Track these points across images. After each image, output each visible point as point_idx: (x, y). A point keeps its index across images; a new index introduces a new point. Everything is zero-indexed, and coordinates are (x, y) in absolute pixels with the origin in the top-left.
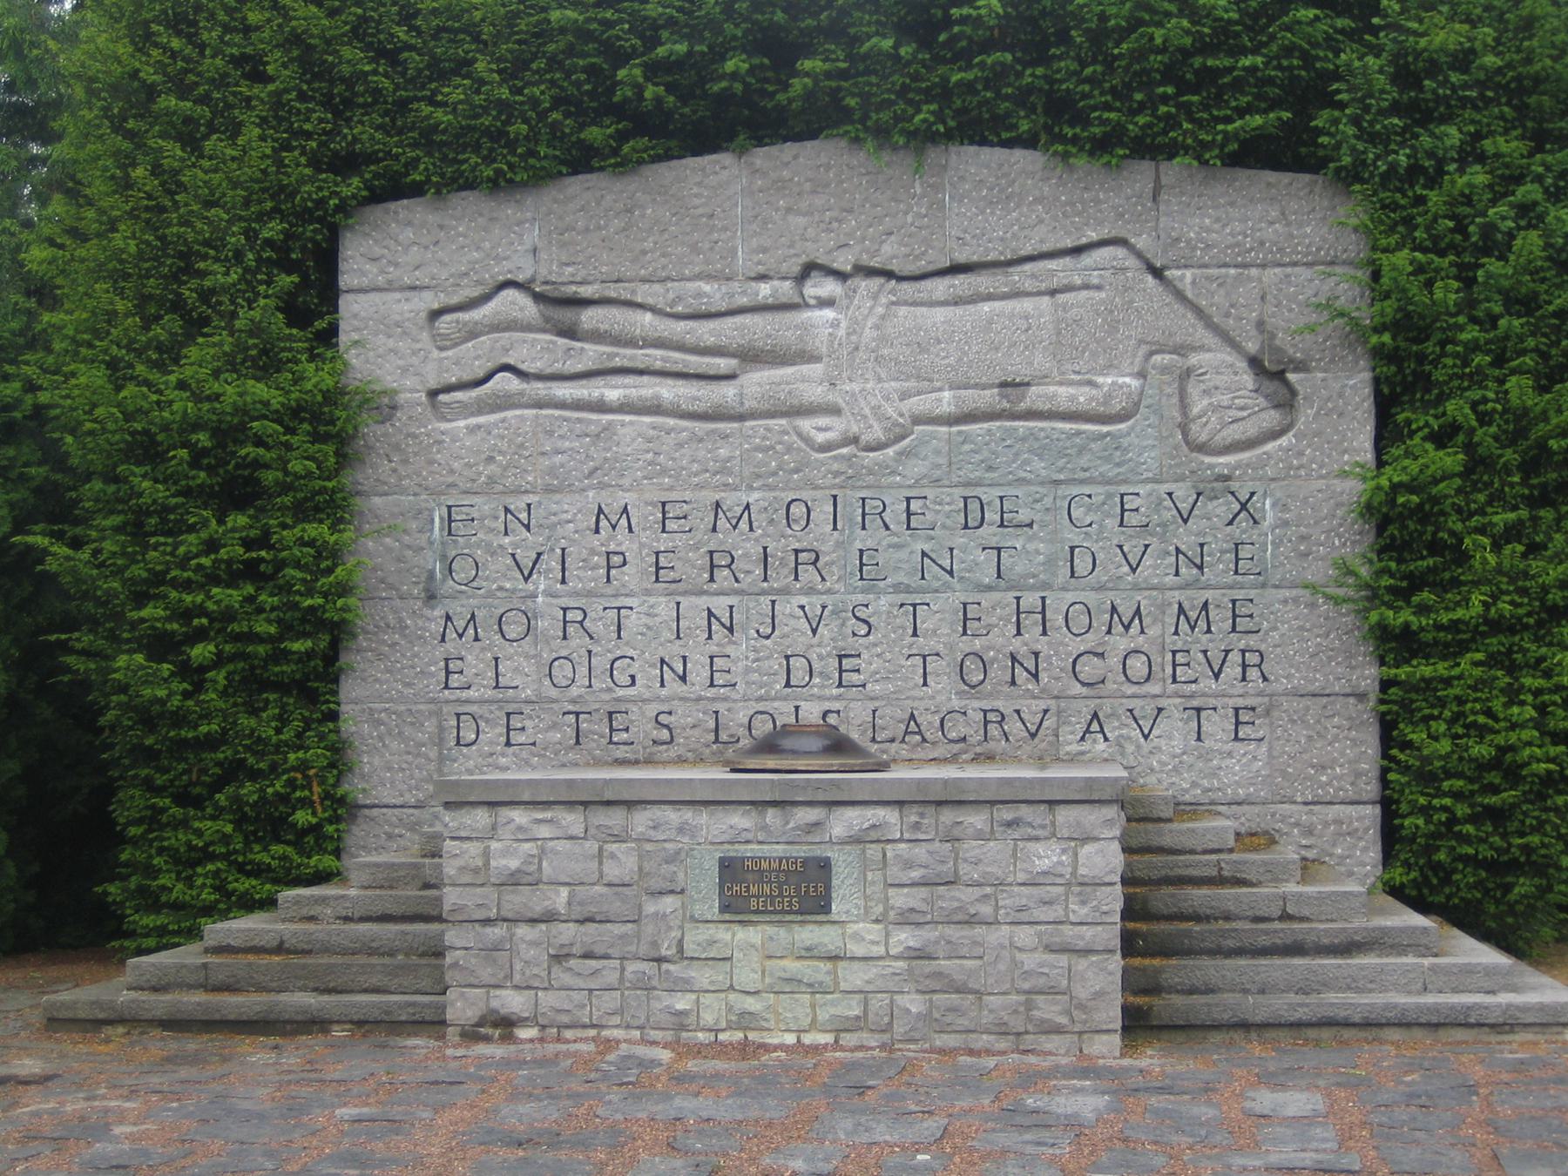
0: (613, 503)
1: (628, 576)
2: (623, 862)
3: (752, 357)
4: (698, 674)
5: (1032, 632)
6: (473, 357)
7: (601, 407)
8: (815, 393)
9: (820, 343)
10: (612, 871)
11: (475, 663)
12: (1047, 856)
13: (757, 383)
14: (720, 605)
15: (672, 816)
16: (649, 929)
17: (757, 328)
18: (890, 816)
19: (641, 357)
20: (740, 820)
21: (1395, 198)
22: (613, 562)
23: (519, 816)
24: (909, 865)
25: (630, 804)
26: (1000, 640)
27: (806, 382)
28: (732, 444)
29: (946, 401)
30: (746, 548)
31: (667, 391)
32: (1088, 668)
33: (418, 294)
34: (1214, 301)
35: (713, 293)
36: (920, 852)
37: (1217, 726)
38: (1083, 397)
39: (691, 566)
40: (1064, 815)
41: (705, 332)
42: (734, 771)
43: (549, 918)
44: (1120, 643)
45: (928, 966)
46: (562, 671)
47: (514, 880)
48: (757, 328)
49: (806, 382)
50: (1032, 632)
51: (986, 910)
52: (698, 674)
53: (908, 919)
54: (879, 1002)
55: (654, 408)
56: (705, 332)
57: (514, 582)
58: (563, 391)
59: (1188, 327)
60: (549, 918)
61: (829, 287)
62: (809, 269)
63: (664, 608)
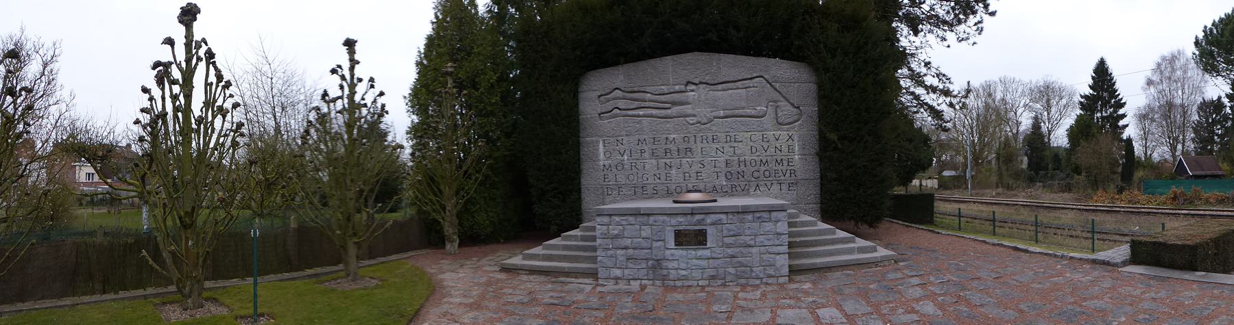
0: (642, 137)
1: (646, 155)
2: (646, 232)
3: (674, 104)
4: (663, 178)
5: (742, 167)
6: (609, 106)
7: (639, 116)
8: (690, 112)
9: (690, 100)
10: (644, 234)
11: (611, 176)
12: (769, 226)
13: (675, 110)
14: (668, 161)
15: (661, 218)
16: (654, 252)
17: (676, 97)
18: (723, 217)
19: (647, 104)
20: (681, 219)
21: (819, 68)
22: (642, 151)
23: (617, 219)
24: (729, 230)
25: (648, 215)
26: (735, 168)
27: (687, 109)
28: (670, 124)
29: (722, 113)
30: (672, 147)
31: (654, 112)
32: (756, 174)
33: (600, 95)
34: (784, 91)
35: (665, 89)
36: (732, 227)
37: (784, 187)
38: (753, 112)
39: (661, 152)
40: (774, 214)
41: (663, 98)
42: (675, 202)
43: (626, 248)
44: (763, 168)
45: (736, 260)
46: (631, 177)
47: (617, 237)
48: (676, 97)
49: (687, 109)
50: (742, 167)
51: (752, 243)
52: (663, 178)
53: (729, 246)
54: (721, 271)
55: (652, 116)
56: (663, 98)
57: (619, 157)
58: (630, 113)
59: (777, 96)
60: (626, 248)
61: (693, 87)
62: (688, 83)
63: (654, 161)
